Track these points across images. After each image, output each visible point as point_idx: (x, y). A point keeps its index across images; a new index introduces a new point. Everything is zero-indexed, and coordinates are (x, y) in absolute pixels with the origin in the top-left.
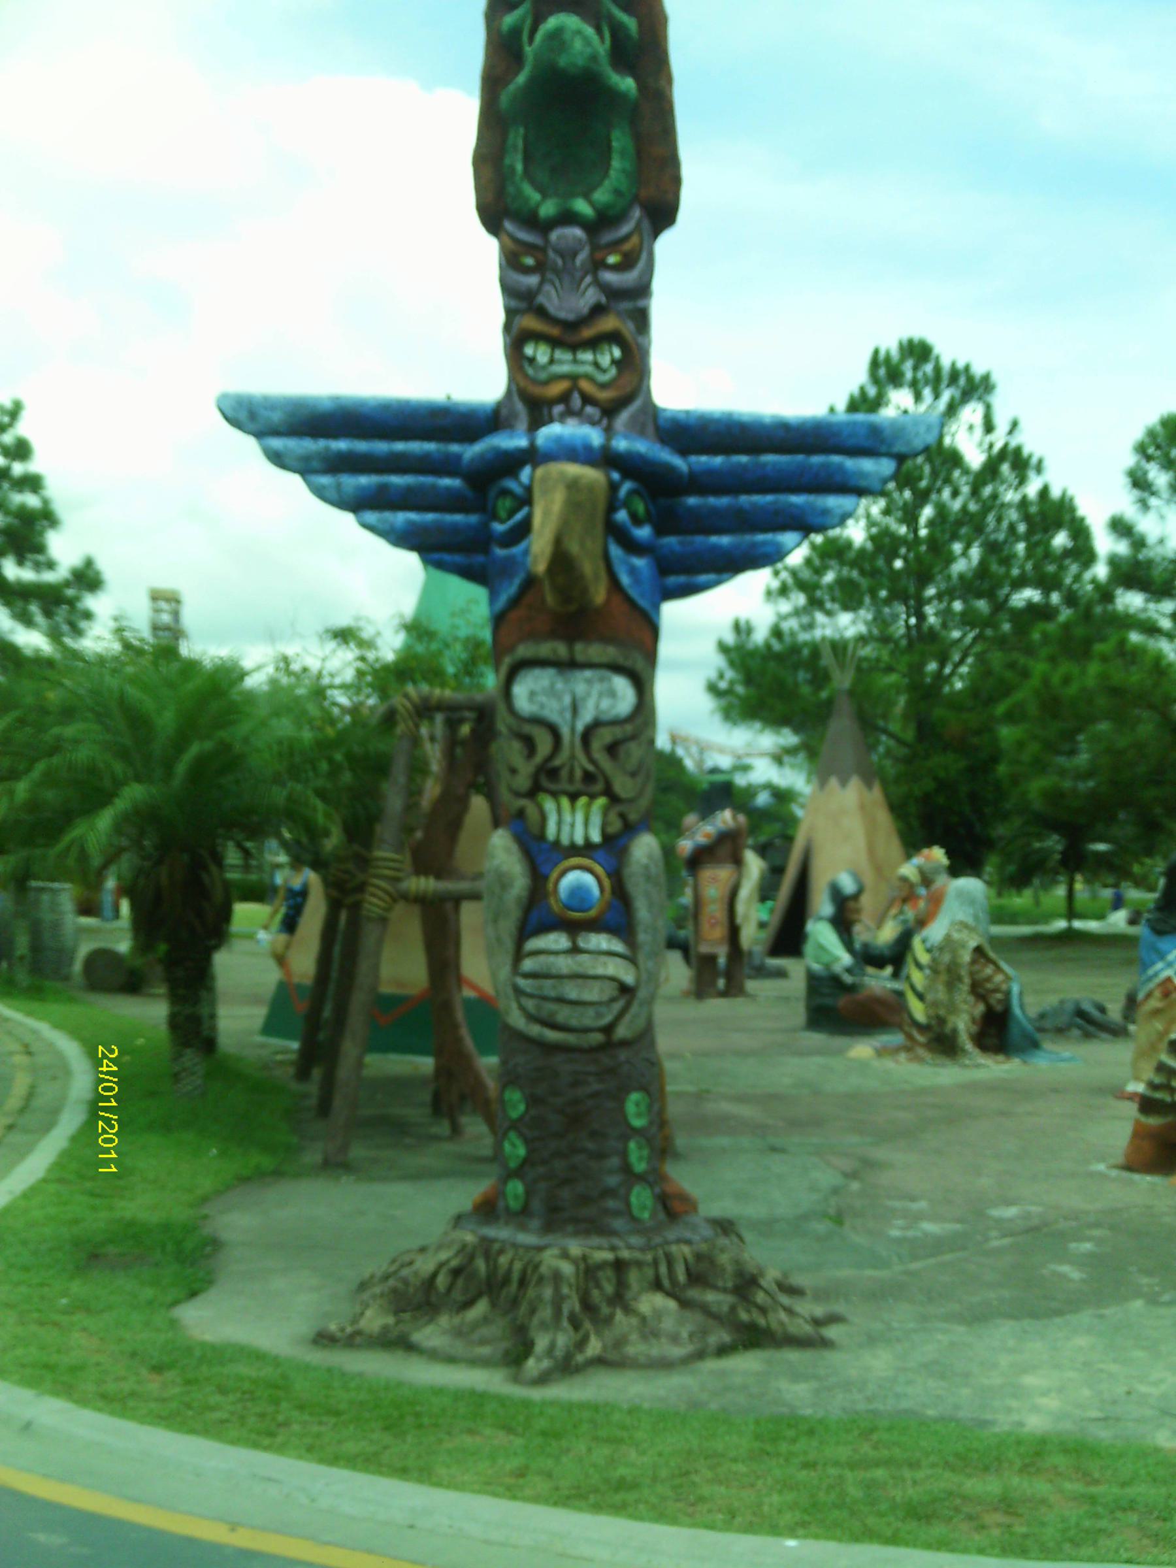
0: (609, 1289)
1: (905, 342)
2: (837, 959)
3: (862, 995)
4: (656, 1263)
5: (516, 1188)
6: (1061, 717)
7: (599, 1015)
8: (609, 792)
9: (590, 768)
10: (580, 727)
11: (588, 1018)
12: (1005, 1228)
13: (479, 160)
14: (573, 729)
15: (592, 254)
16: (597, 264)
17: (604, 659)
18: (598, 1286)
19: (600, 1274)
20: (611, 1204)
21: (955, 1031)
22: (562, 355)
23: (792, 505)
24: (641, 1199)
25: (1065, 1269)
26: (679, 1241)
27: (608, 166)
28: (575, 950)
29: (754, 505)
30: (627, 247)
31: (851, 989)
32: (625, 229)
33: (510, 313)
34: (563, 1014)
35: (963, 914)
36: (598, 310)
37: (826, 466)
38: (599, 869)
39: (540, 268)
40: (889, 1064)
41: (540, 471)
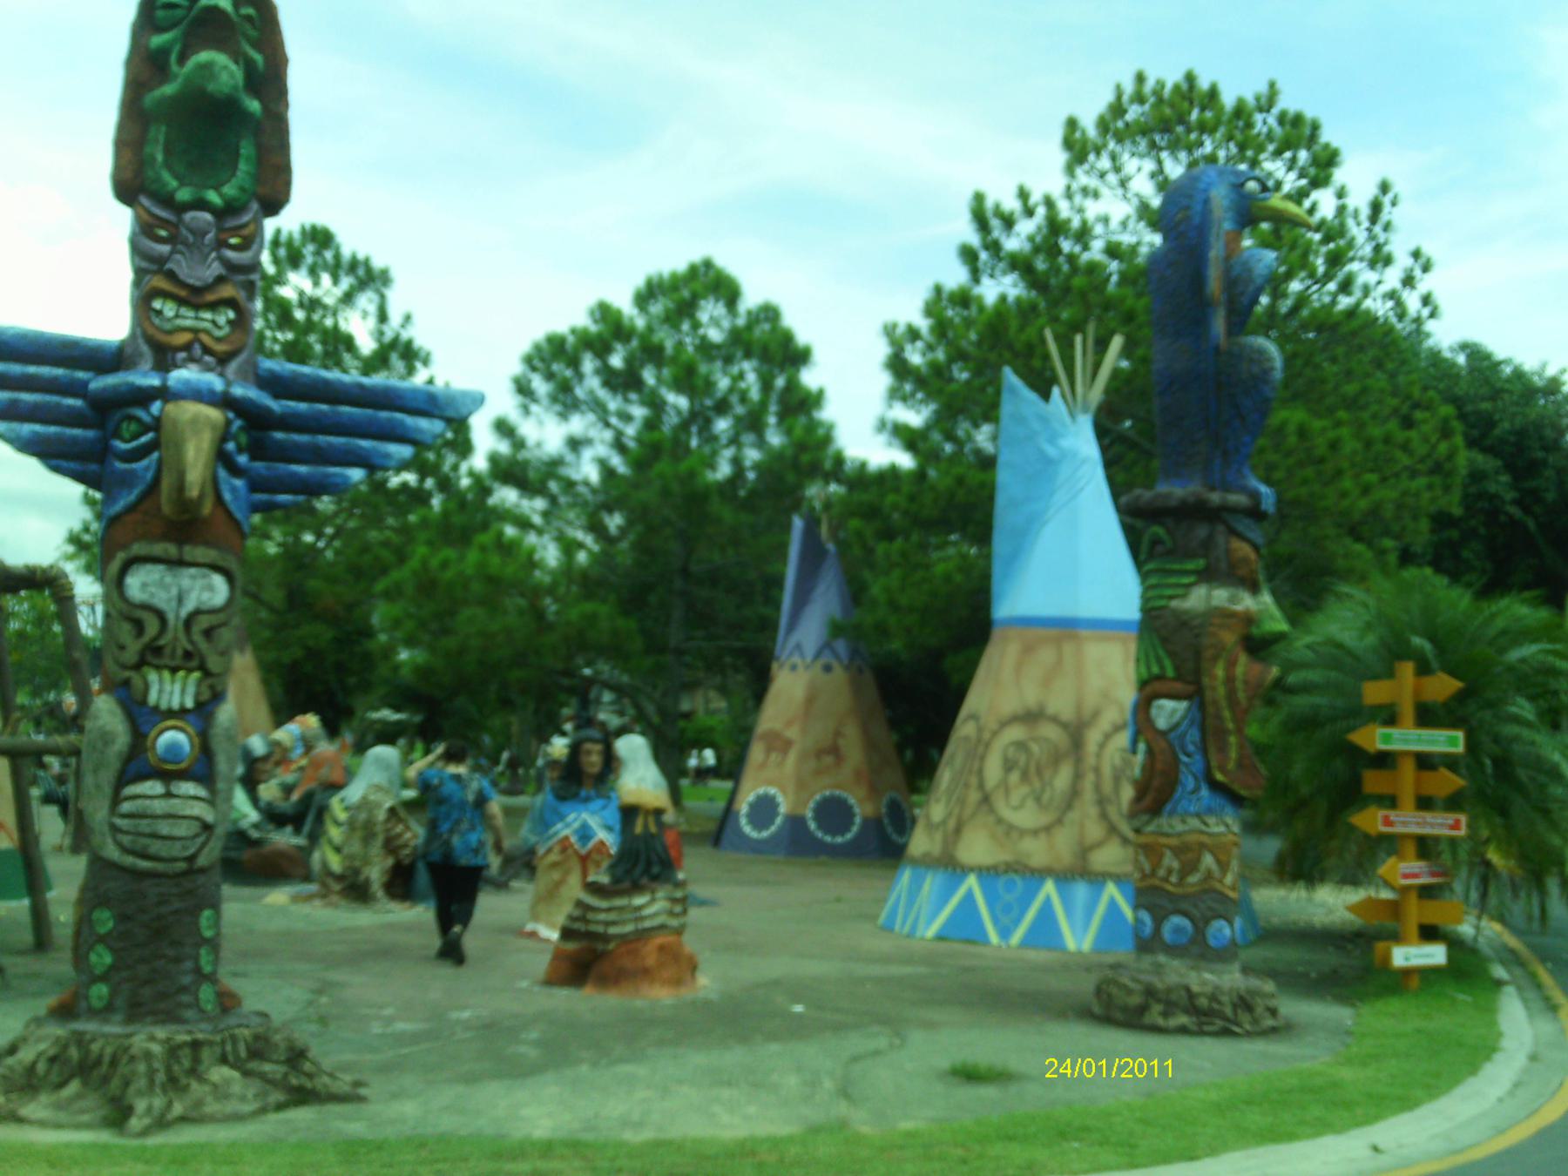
0: (187, 1063)
1: (308, 227)
2: (245, 816)
3: (266, 849)
4: (223, 1042)
5: (100, 991)
6: (436, 603)
7: (185, 848)
8: (202, 667)
9: (189, 647)
10: (184, 613)
11: (176, 850)
12: (466, 1025)
13: (121, 144)
14: (177, 617)
15: (217, 235)
16: (221, 244)
17: (207, 560)
18: (179, 1063)
19: (181, 1053)
20: (185, 998)
21: (367, 883)
22: (187, 312)
23: (361, 448)
24: (206, 993)
25: (523, 1049)
26: (239, 1026)
27: (235, 168)
28: (169, 795)
29: (330, 445)
30: (246, 232)
31: (256, 843)
32: (246, 218)
33: (140, 273)
34: (156, 847)
35: (379, 778)
36: (220, 280)
37: (389, 420)
38: (190, 729)
39: (171, 240)
40: (305, 909)
41: (170, 407)
